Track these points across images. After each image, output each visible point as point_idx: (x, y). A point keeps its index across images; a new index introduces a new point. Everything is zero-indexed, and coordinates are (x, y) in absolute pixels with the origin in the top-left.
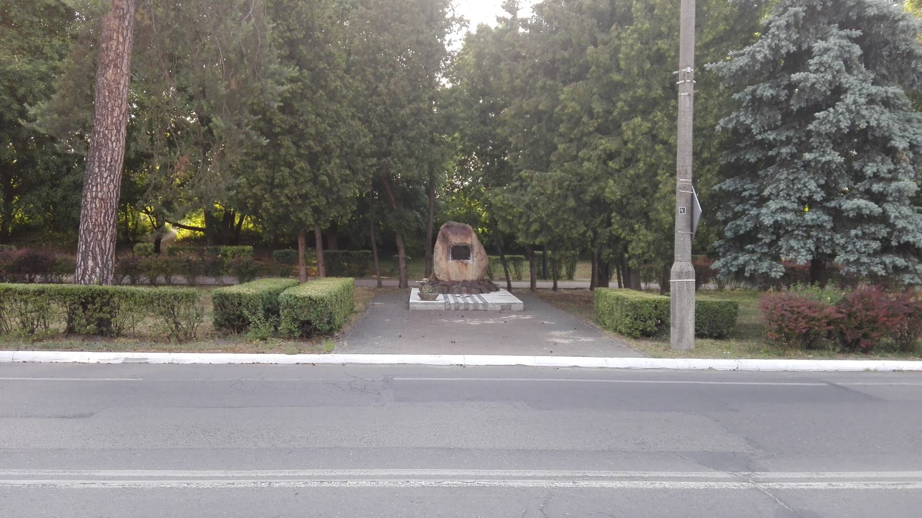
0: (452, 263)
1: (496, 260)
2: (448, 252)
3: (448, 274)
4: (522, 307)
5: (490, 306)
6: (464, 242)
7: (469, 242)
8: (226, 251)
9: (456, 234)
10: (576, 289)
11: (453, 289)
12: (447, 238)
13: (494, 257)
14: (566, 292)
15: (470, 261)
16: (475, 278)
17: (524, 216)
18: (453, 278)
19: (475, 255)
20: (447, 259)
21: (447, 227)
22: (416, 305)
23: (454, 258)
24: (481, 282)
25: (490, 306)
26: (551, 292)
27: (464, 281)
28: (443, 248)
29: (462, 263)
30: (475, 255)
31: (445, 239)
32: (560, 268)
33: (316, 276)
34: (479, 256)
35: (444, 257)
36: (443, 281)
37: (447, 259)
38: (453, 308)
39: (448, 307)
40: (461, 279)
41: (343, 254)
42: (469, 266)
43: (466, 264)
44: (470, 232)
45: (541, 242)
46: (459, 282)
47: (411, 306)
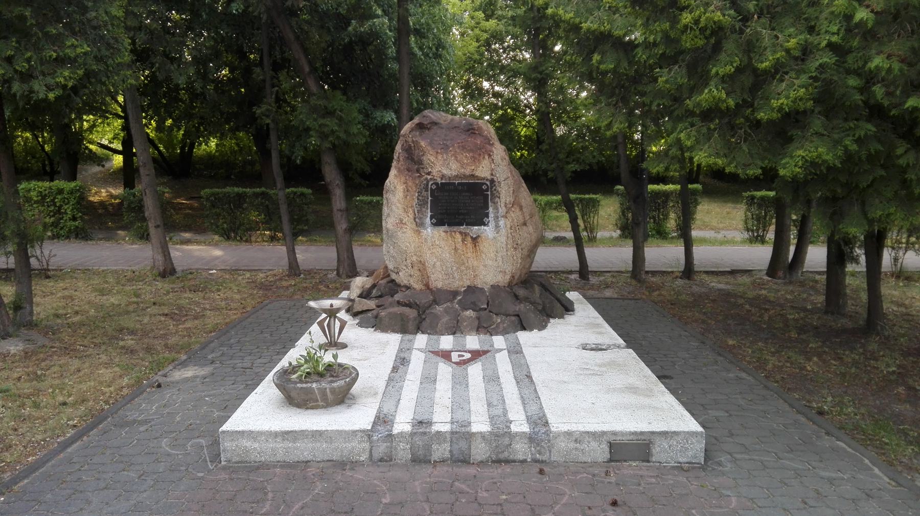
0: (434, 235)
1: (549, 204)
2: (422, 204)
3: (422, 267)
4: (696, 450)
5: (562, 444)
6: (468, 172)
7: (483, 171)
8: (29, 190)
9: (445, 148)
10: (733, 272)
11: (437, 318)
12: (420, 162)
13: (544, 199)
14: (716, 284)
15: (488, 231)
16: (502, 279)
17: (729, 45)
18: (438, 281)
19: (502, 210)
20: (420, 224)
21: (421, 127)
22: (247, 443)
23: (440, 220)
24: (521, 292)
25: (562, 444)
26: (679, 282)
27: (471, 290)
28: (407, 190)
29: (464, 235)
30: (502, 210)
31: (415, 162)
32: (666, 217)
33: (378, 206)
34: (515, 214)
35: (408, 219)
36: (408, 288)
37: (420, 224)
38: (403, 452)
39: (381, 449)
40: (460, 283)
41: (256, 195)
42: (484, 246)
43: (475, 240)
44: (488, 141)
45: (812, 165)
46: (455, 293)
47: (227, 444)
